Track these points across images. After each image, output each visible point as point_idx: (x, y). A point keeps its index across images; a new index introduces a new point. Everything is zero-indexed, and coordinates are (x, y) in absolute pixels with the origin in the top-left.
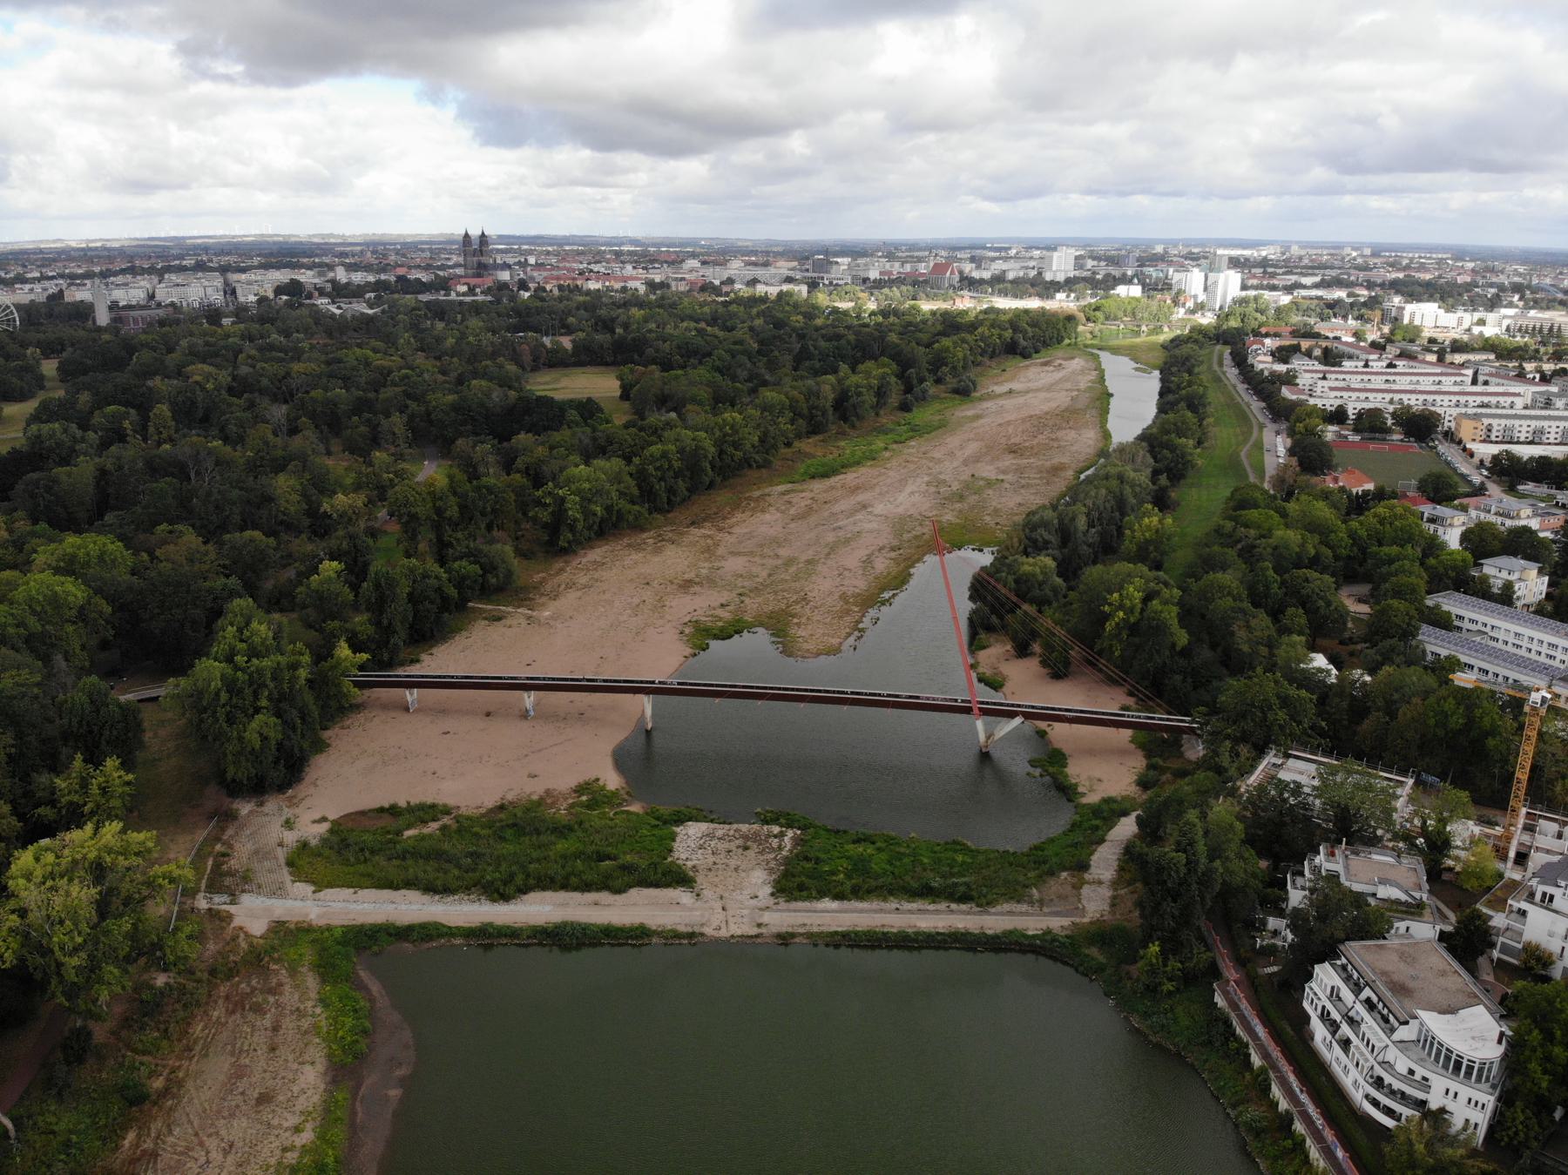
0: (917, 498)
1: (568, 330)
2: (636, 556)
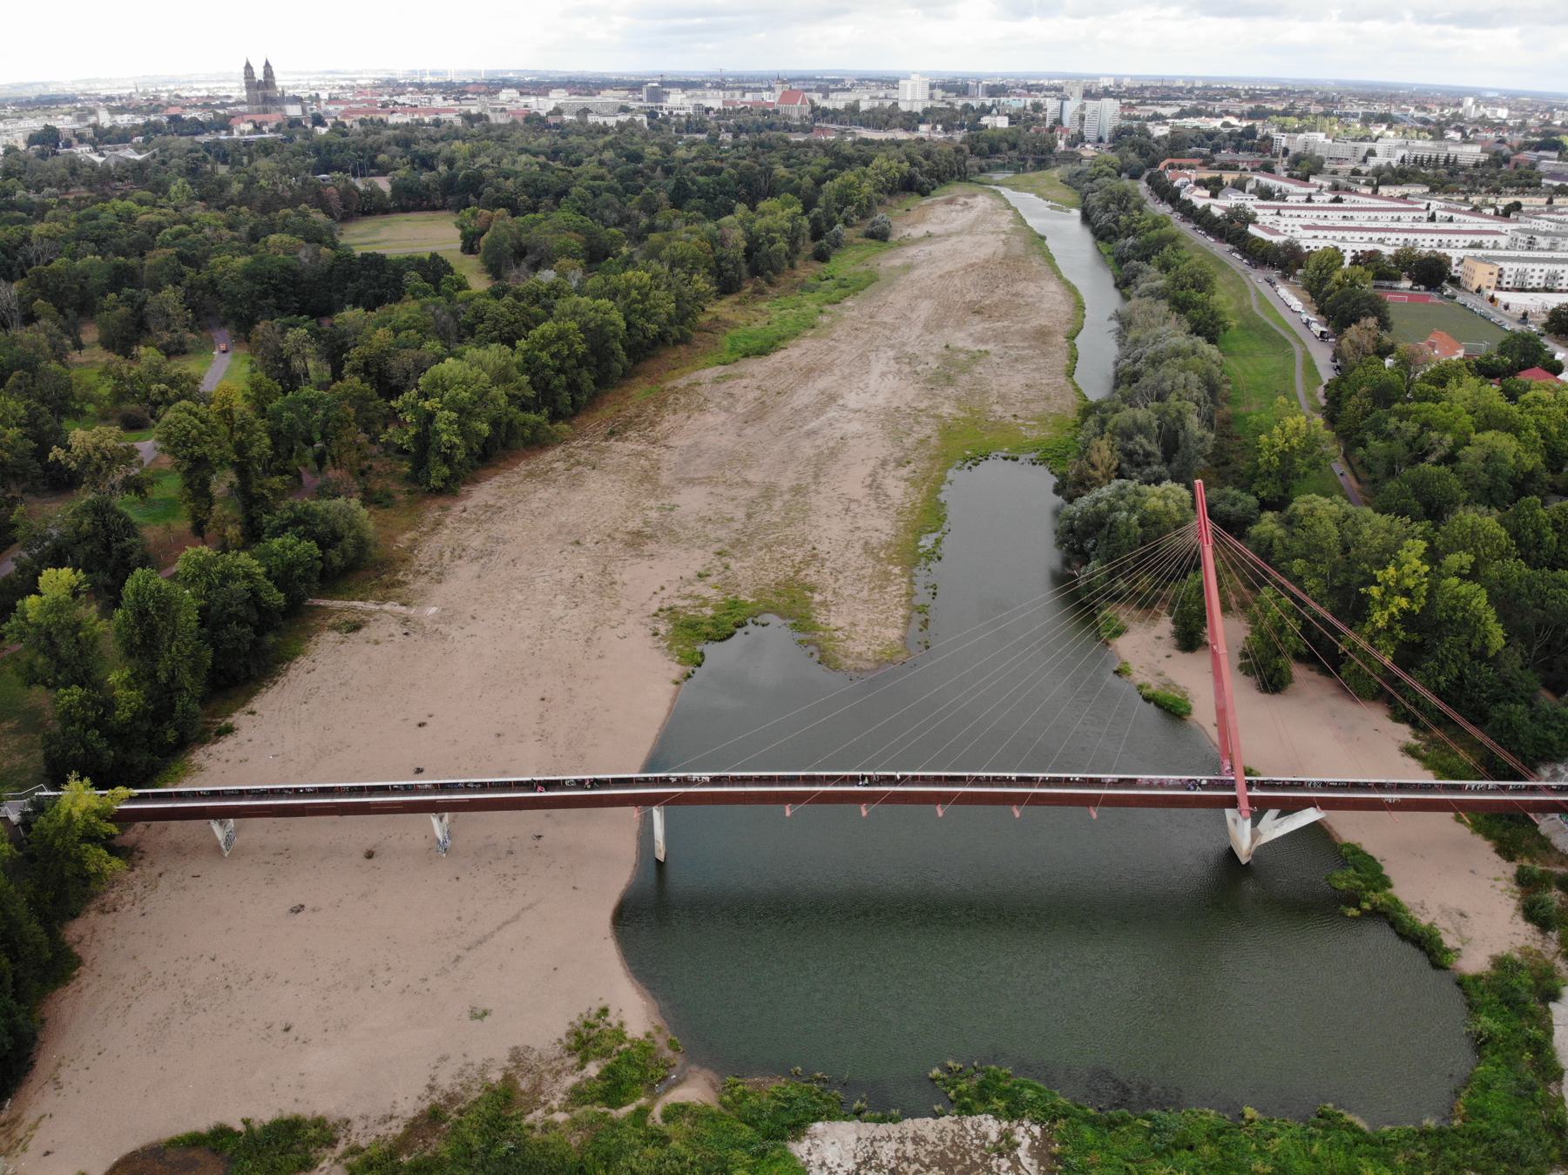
0: (892, 382)
1: (383, 171)
2: (547, 493)
